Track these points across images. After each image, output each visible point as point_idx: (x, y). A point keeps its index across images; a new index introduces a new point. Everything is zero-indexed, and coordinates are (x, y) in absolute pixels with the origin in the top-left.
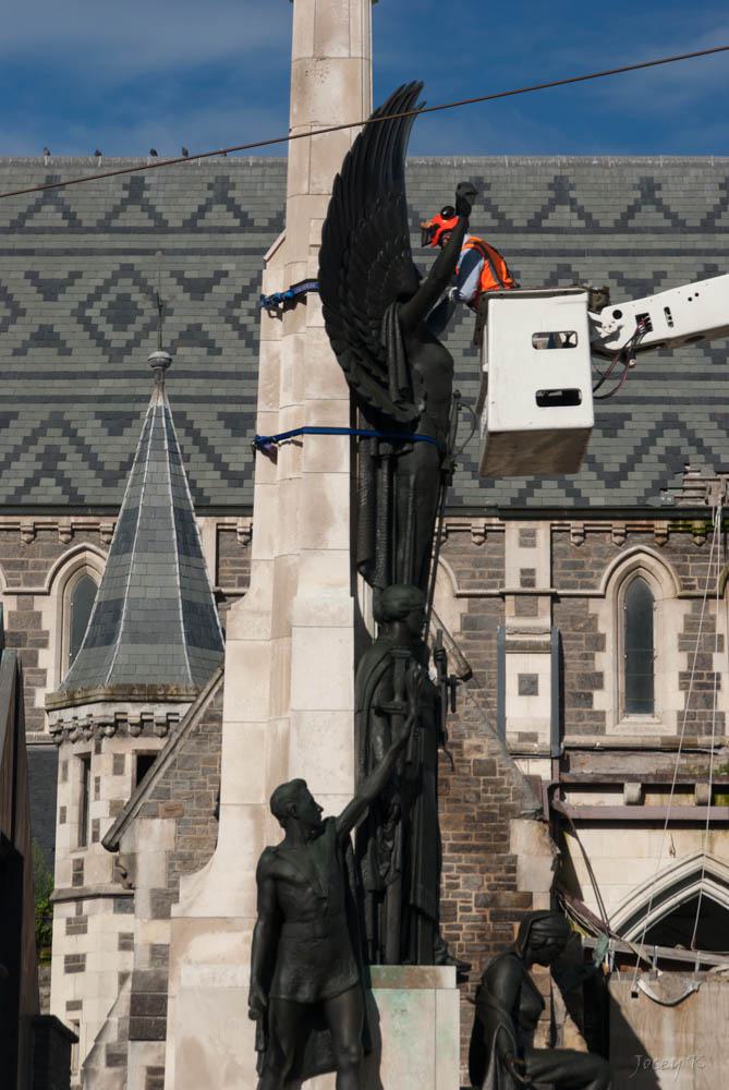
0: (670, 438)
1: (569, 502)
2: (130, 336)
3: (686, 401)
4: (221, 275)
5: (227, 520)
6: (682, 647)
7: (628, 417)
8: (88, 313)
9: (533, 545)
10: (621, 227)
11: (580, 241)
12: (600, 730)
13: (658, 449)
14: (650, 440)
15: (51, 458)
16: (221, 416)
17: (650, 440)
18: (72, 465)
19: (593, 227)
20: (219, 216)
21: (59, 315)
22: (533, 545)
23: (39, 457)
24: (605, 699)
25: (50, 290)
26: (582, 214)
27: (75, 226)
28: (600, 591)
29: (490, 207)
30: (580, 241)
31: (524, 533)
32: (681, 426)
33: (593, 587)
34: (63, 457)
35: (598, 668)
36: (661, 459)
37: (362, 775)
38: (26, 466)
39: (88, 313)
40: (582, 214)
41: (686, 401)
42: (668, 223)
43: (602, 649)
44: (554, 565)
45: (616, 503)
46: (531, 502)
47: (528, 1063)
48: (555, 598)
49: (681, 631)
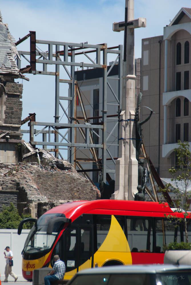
37: (60, 215)
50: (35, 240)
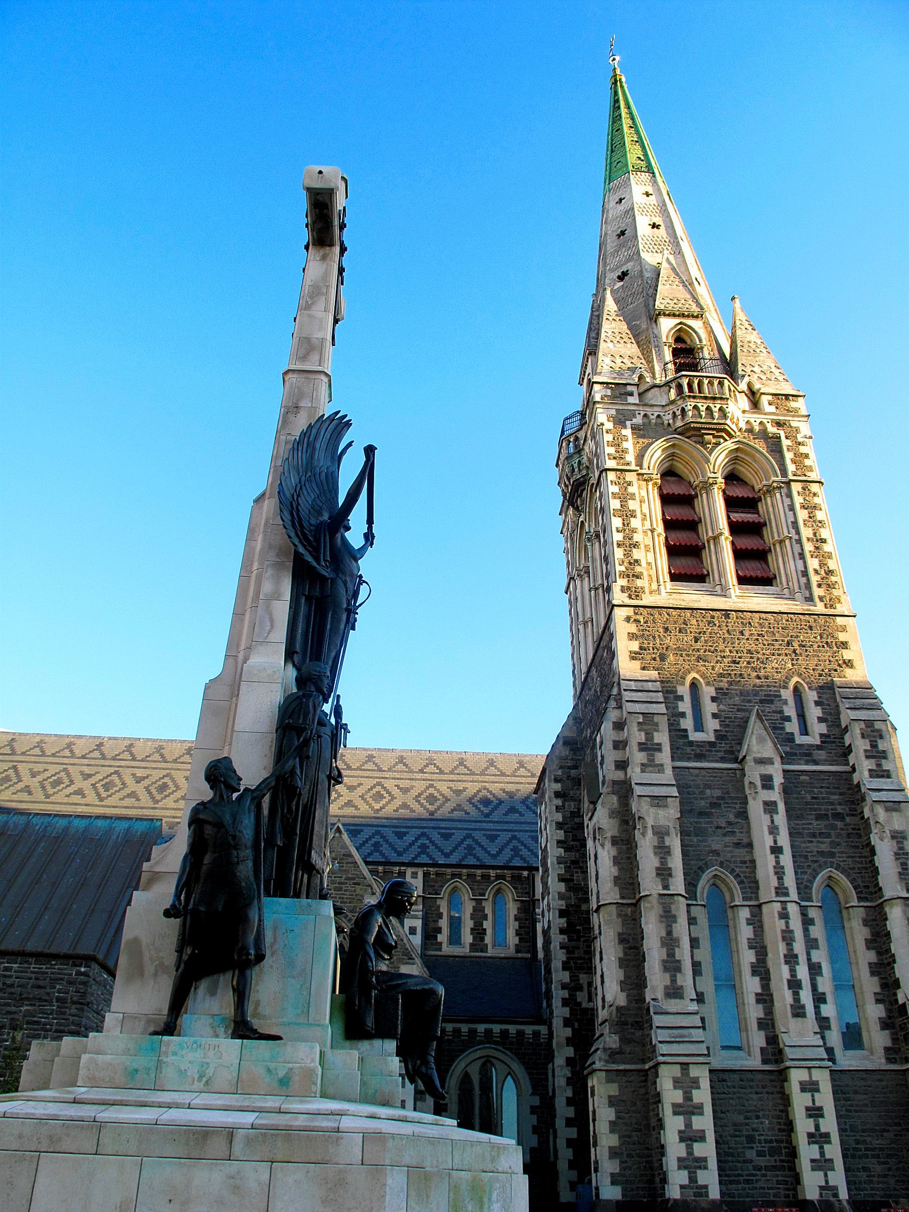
0: (469, 842)
1: (478, 863)
2: (56, 790)
3: (475, 829)
4: (360, 785)
5: (387, 867)
6: (471, 919)
7: (499, 836)
8: (175, 789)
9: (417, 878)
10: (452, 773)
11: (435, 777)
12: (440, 950)
13: (511, 846)
14: (370, 838)
15: (376, 845)
16: (484, 835)
17: (370, 838)
18: (385, 848)
19: (441, 772)
20: (400, 767)
21: (140, 789)
22: (417, 878)
23: (372, 845)
24: (442, 938)
25: (139, 780)
26: (438, 768)
27: (134, 759)
28: (486, 897)
29: (344, 761)
30: (435, 777)
31: (413, 873)
32: (473, 838)
33: (484, 895)
34: (474, 849)
35: (440, 926)
36: (511, 850)
38: (415, 849)
39: (175, 789)
40: (438, 768)
41: (475, 829)
42: (438, 771)
43: (442, 918)
44: (669, 897)
45: (448, 863)
46: (463, 863)
47: (850, 1159)
48: (424, 897)
49: (472, 912)
50: (462, 930)
